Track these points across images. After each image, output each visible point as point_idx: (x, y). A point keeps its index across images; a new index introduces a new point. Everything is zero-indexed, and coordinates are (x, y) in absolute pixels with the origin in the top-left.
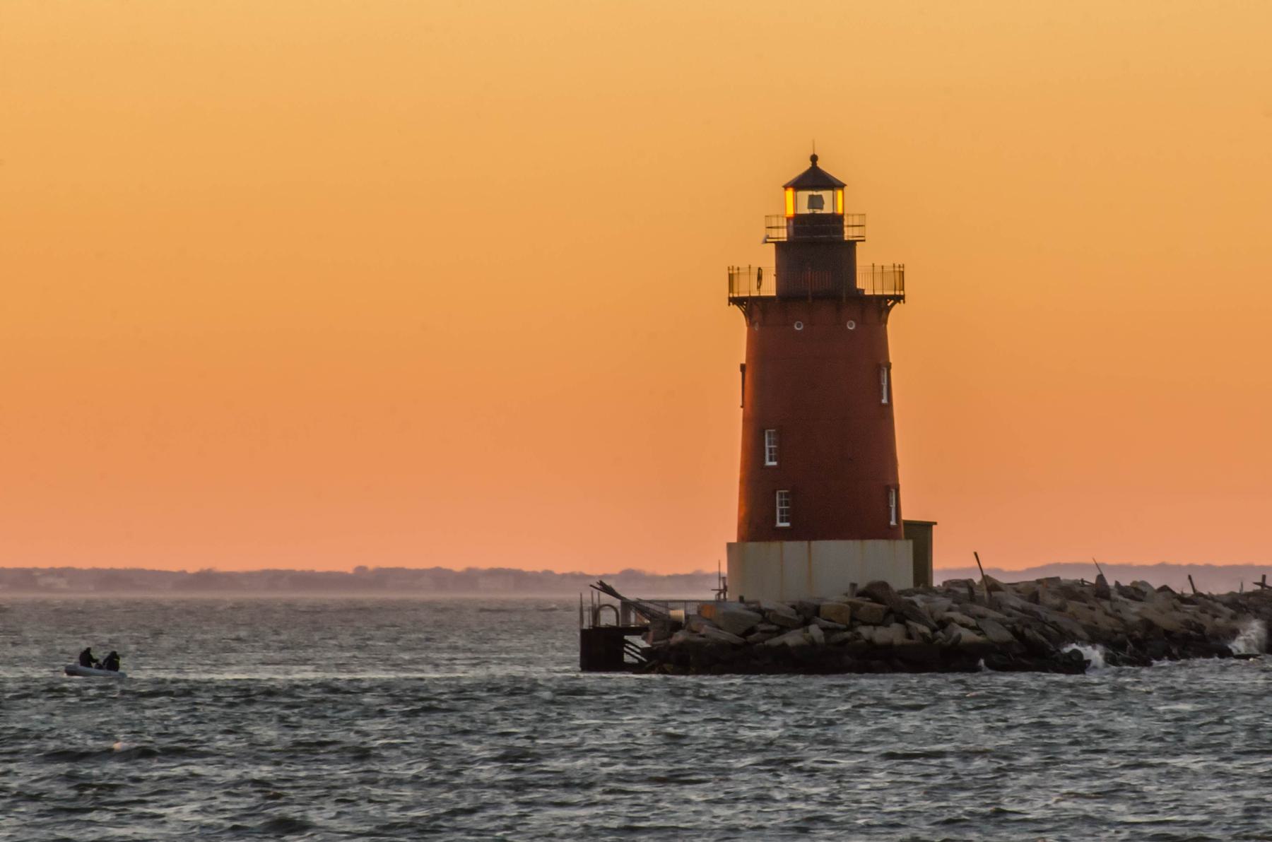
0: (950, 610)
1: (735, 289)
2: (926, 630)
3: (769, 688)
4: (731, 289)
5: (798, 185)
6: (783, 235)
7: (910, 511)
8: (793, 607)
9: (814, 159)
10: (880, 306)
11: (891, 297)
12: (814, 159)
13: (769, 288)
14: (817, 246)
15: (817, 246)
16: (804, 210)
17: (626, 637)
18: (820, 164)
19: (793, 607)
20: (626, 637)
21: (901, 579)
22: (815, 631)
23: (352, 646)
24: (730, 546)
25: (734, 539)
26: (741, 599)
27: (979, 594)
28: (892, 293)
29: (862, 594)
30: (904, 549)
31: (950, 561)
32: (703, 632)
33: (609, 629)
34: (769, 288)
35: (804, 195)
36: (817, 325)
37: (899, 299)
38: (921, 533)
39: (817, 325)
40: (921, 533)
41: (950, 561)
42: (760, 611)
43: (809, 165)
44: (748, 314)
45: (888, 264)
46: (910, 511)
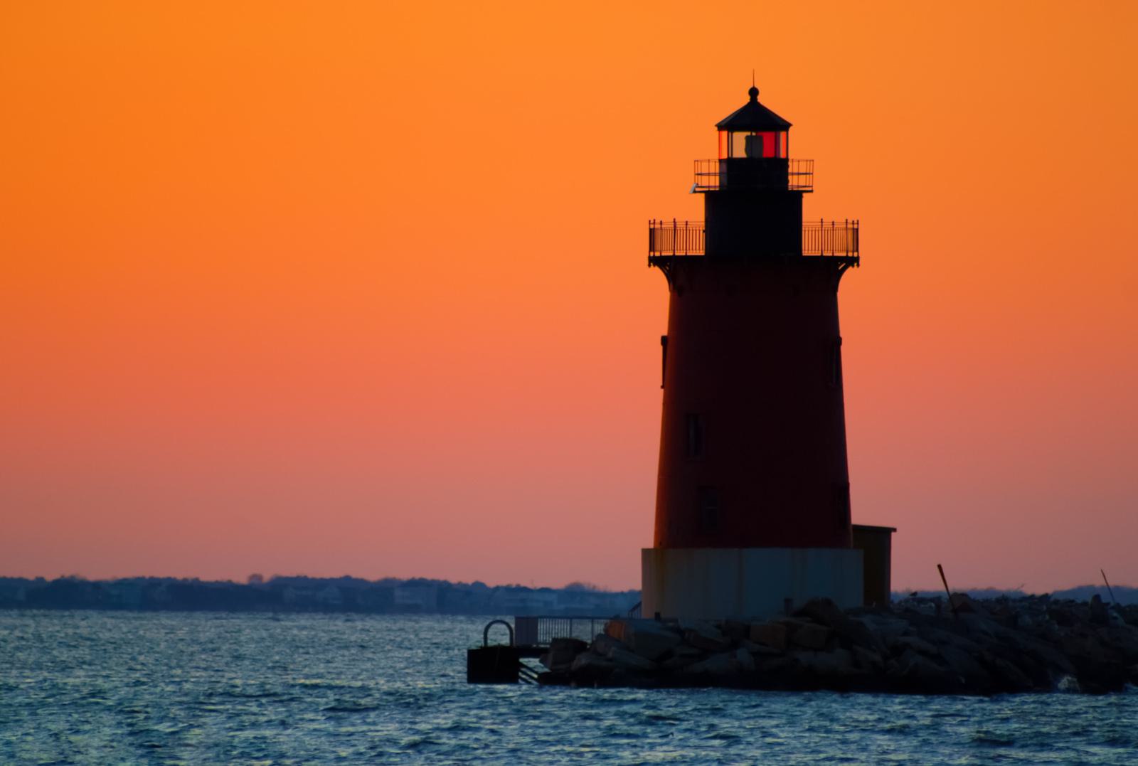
0: (906, 633)
1: (658, 246)
2: (877, 657)
3: (257, 717)
4: (652, 247)
5: (729, 125)
6: (714, 182)
7: (863, 512)
8: (719, 627)
9: (754, 92)
10: (830, 270)
11: (841, 259)
12: (754, 92)
13: (697, 248)
14: (755, 188)
15: (755, 188)
16: (740, 152)
17: (523, 660)
18: (762, 99)
19: (719, 627)
20: (523, 660)
21: (851, 597)
22: (743, 655)
23: (612, 758)
24: (645, 552)
25: (650, 543)
26: (658, 616)
27: (956, 611)
28: (844, 254)
29: (800, 613)
30: (853, 560)
31: (909, 574)
32: (610, 655)
33: (500, 649)
34: (697, 248)
35: (740, 138)
36: (753, 297)
37: (853, 261)
38: (878, 539)
39: (753, 297)
40: (878, 539)
41: (909, 574)
42: (680, 632)
43: (746, 99)
44: (671, 277)
45: (840, 219)
46: (863, 512)
